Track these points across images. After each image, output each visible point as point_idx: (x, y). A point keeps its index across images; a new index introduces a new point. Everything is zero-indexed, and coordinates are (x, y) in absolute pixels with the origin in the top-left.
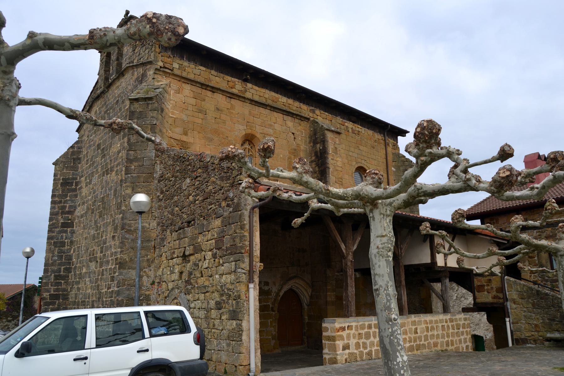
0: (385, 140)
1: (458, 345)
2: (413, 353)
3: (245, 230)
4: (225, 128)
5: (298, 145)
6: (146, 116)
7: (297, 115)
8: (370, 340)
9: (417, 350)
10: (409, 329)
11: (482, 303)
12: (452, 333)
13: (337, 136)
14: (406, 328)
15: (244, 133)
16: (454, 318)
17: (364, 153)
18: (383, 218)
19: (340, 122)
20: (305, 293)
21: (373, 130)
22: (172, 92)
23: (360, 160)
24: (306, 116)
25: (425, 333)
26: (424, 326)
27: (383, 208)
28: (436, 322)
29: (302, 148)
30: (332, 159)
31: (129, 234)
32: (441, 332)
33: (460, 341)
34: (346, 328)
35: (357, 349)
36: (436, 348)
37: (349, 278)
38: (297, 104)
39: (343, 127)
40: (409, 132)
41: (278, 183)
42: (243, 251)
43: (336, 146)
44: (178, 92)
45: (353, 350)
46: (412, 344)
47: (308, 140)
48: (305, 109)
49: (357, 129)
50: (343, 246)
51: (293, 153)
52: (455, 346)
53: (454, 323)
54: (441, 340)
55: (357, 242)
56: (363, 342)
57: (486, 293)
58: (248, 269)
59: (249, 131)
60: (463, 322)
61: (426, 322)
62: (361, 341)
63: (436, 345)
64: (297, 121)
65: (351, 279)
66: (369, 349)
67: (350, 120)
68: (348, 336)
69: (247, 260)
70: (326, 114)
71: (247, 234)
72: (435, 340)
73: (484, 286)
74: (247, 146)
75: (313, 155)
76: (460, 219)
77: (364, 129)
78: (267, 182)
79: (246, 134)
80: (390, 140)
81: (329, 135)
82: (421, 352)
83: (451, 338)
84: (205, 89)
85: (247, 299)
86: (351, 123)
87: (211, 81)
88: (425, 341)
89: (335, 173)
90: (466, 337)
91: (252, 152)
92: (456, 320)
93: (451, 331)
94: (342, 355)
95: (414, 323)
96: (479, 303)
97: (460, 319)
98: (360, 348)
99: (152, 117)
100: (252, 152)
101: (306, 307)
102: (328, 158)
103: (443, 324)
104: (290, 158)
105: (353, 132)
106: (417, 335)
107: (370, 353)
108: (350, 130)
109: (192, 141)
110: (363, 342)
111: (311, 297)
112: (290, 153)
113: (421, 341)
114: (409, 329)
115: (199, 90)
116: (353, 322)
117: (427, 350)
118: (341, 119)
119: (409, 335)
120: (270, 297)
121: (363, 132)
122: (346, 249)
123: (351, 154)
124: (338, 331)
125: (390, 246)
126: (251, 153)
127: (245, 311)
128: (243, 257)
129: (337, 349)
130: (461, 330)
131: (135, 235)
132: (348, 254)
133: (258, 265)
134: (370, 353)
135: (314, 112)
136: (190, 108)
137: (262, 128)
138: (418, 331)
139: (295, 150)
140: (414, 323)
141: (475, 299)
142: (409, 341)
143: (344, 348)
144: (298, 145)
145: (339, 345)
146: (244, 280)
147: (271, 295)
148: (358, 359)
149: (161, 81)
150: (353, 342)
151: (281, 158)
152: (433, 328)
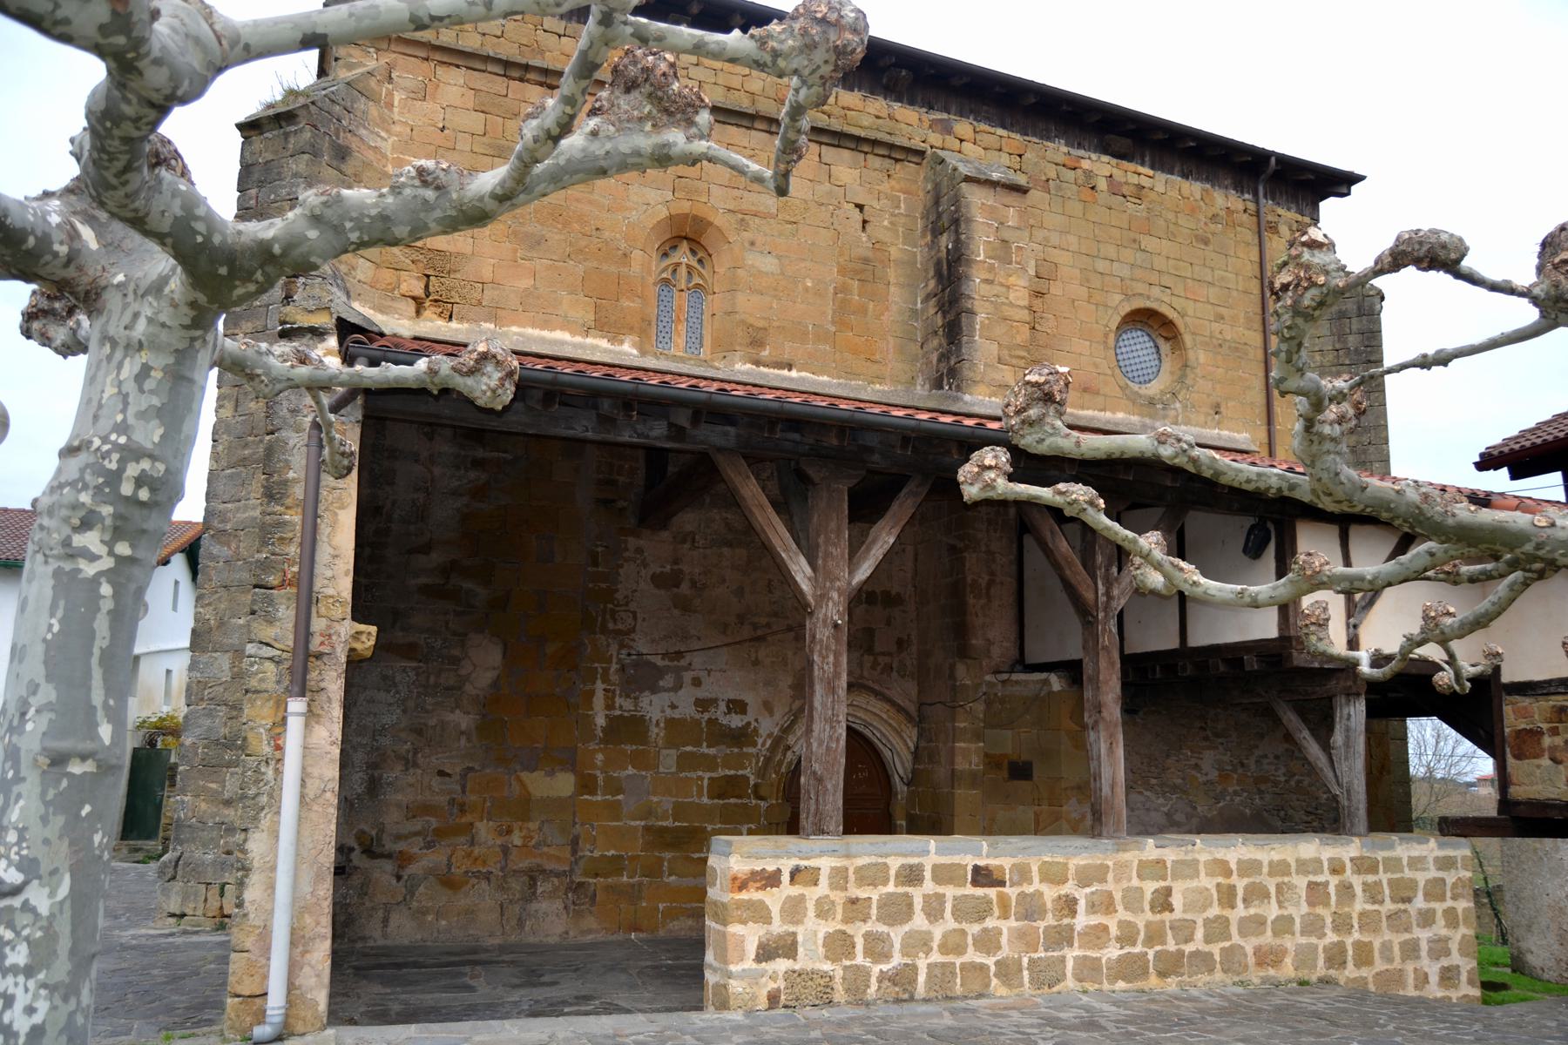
0: (1258, 214)
1: (1397, 964)
2: (1139, 985)
3: (289, 502)
4: (590, 202)
5: (877, 244)
6: (279, 173)
7: (875, 143)
8: (906, 928)
9: (1162, 974)
10: (1127, 891)
11: (1532, 804)
12: (1362, 915)
13: (1012, 198)
14: (1110, 886)
15: (664, 213)
16: (1380, 855)
17: (1159, 263)
18: (109, 358)
19: (1060, 159)
20: (895, 740)
21: (1207, 180)
22: (398, 97)
23: (1140, 288)
24: (916, 143)
25: (1214, 911)
26: (1208, 882)
27: (125, 306)
28: (1280, 868)
29: (894, 252)
30: (986, 281)
31: (220, 543)
32: (1305, 908)
33: (1410, 950)
34: (786, 878)
35: (832, 956)
36: (1272, 972)
37: (819, 689)
38: (878, 105)
39: (1070, 175)
40: (1360, 178)
41: (794, 374)
42: (273, 580)
43: (1006, 235)
44: (421, 94)
45: (812, 957)
46: (1138, 949)
47: (920, 224)
48: (910, 122)
49: (1134, 179)
50: (801, 570)
51: (856, 272)
52: (1380, 965)
53: (1383, 877)
54: (1304, 940)
55: (877, 553)
56: (867, 936)
57: (1545, 762)
58: (291, 643)
59: (685, 207)
60: (1433, 873)
61: (1223, 868)
62: (858, 931)
63: (1268, 957)
64: (876, 162)
65: (832, 690)
66: (897, 960)
67: (1105, 150)
68: (794, 910)
69: (286, 613)
70: (1000, 131)
71: (294, 517)
72: (1267, 938)
73: (1540, 733)
74: (683, 256)
75: (932, 273)
76: (1033, 412)
77: (1161, 177)
78: (747, 373)
79: (671, 217)
80: (1280, 211)
81: (977, 200)
82: (1179, 984)
83: (1356, 935)
84: (521, 80)
85: (278, 754)
86: (1106, 158)
87: (542, 52)
88: (1208, 939)
89: (999, 330)
90: (1444, 932)
91: (701, 275)
92: (1393, 864)
93: (1360, 905)
94: (753, 978)
95: (1155, 869)
96: (1518, 803)
97: (1416, 863)
98: (850, 954)
99: (296, 175)
100: (701, 275)
101: (901, 788)
102: (968, 278)
103: (1320, 879)
104: (841, 289)
105: (1115, 188)
106: (1167, 916)
107: (902, 979)
108: (1102, 184)
109: (468, 250)
110: (867, 936)
111: (916, 755)
112: (842, 271)
113: (1189, 939)
114: (1127, 891)
115: (499, 84)
116: (822, 854)
117: (1219, 975)
118: (1065, 149)
119: (1123, 914)
120: (751, 750)
121: (1160, 188)
122: (814, 581)
123: (1101, 265)
124: (743, 886)
125: (85, 498)
126: (697, 280)
127: (264, 799)
128: (270, 601)
129: (731, 954)
130: (1419, 902)
131: (233, 546)
132: (823, 597)
133: (343, 632)
134: (902, 979)
135: (947, 129)
136: (464, 144)
137: (737, 193)
138: (1177, 900)
139: (866, 261)
140: (1054, 875)
141: (1503, 778)
142: (1118, 939)
143: (766, 953)
144: (877, 244)
145: (741, 940)
146: (270, 685)
147: (755, 744)
148: (839, 995)
149: (361, 64)
150: (813, 932)
151: (807, 289)
152: (1256, 894)
